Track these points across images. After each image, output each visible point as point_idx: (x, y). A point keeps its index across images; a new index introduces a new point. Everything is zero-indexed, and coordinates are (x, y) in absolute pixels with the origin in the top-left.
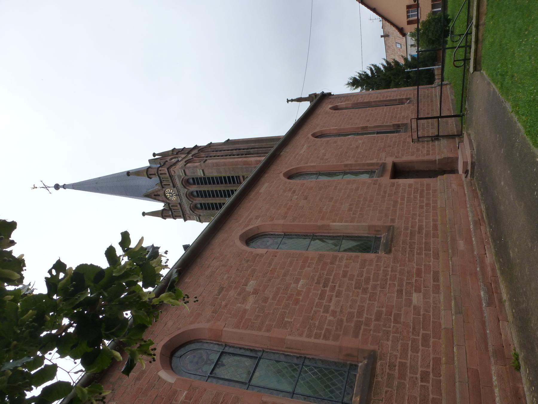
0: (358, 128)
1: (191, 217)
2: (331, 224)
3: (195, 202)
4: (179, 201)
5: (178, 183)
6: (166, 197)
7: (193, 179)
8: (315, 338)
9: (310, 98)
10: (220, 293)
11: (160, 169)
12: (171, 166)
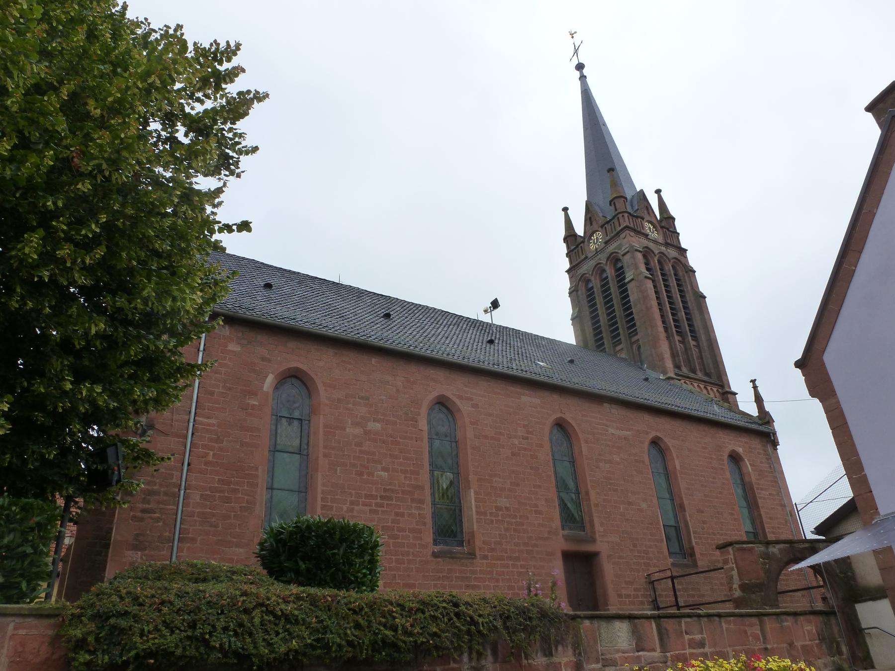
0: (681, 499)
1: (573, 279)
2: (472, 491)
3: (592, 278)
4: (590, 255)
5: (612, 248)
6: (592, 235)
7: (622, 267)
8: (322, 498)
9: (765, 418)
10: (362, 398)
11: (626, 215)
12: (634, 230)
